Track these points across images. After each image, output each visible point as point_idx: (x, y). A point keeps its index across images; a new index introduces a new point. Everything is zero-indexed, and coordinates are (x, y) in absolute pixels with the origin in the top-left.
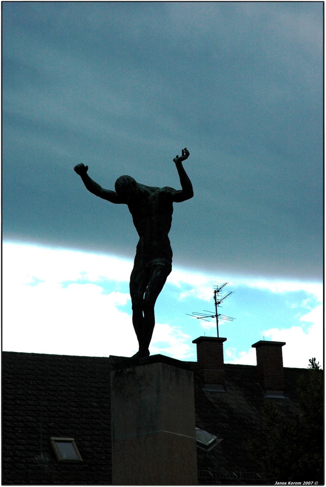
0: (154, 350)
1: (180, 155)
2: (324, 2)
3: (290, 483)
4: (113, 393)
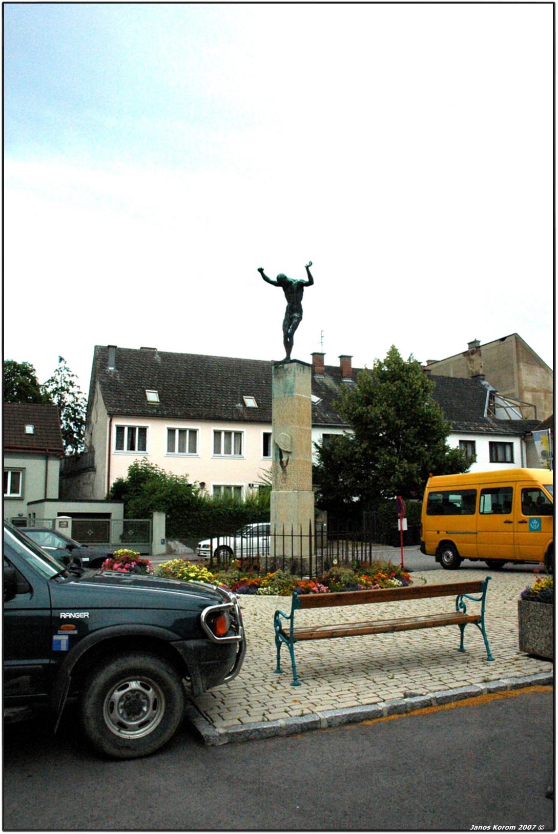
0: (292, 357)
1: (308, 264)
2: (554, 4)
3: (497, 827)
4: (273, 376)
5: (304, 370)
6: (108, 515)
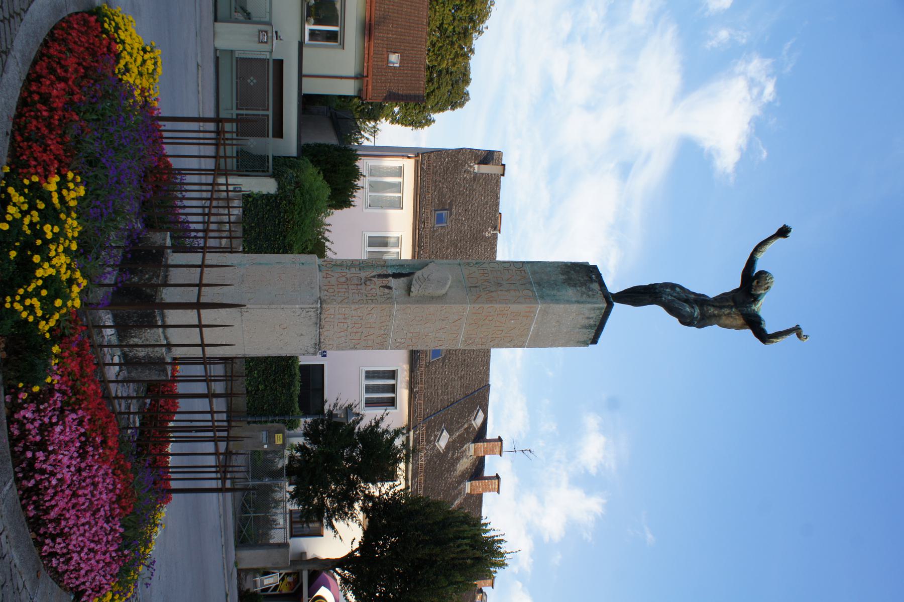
5: (585, 327)
6: (279, 132)
